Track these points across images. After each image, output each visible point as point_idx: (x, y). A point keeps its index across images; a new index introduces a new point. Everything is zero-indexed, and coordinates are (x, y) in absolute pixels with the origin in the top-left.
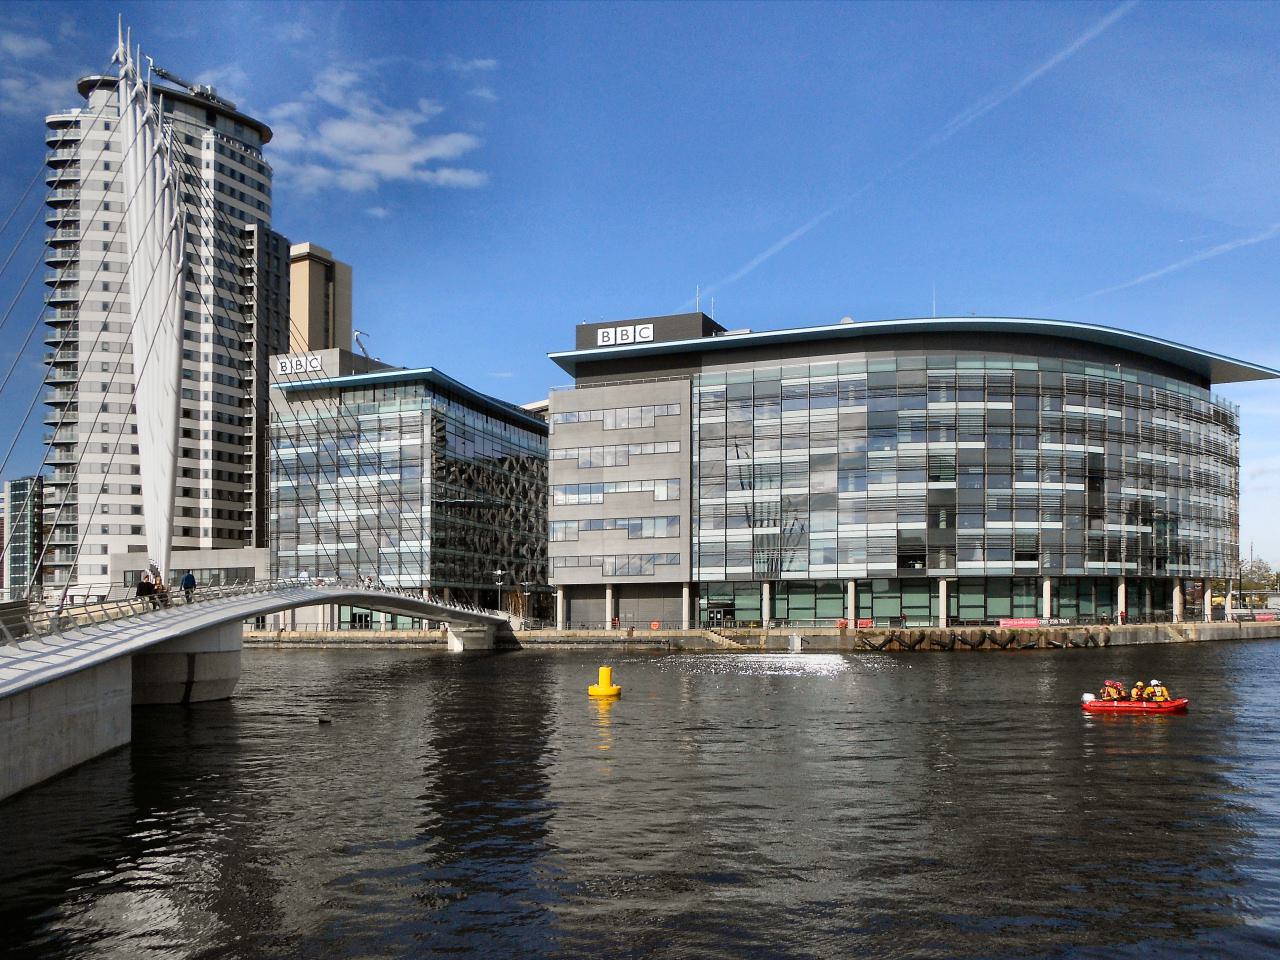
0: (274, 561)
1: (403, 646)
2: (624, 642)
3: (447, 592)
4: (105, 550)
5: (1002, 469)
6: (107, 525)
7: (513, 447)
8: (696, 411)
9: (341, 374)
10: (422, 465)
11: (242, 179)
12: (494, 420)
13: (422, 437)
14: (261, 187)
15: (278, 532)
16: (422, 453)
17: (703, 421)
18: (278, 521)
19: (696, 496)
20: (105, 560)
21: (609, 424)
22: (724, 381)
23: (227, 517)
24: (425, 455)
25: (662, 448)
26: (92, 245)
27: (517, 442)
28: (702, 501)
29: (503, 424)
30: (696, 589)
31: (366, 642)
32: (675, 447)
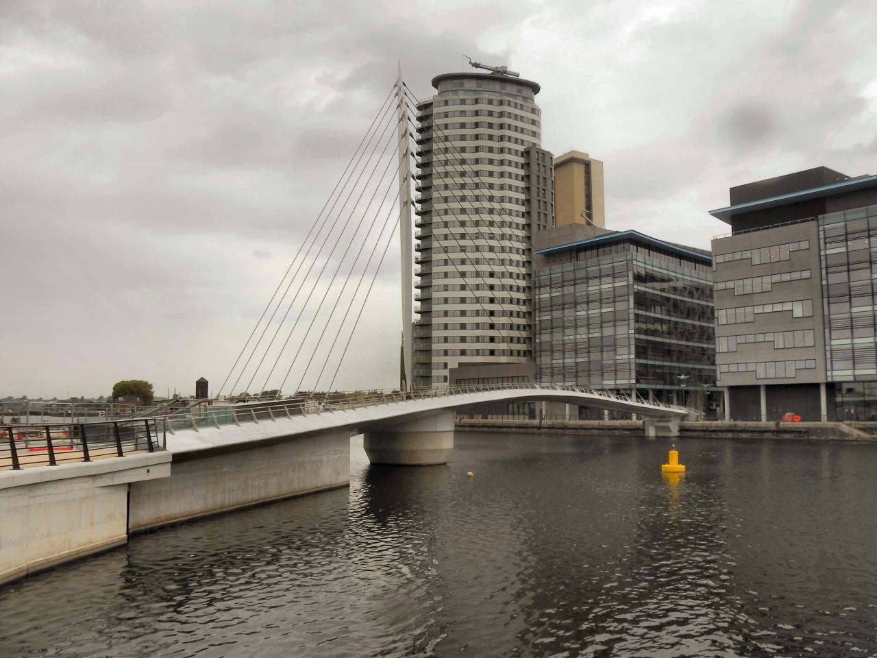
0: (538, 371)
1: (617, 433)
2: (773, 432)
3: (651, 395)
4: (446, 365)
5: (832, 239)
6: (447, 112)
7: (685, 277)
8: (822, 246)
9: (732, 204)
10: (628, 276)
11: (522, 131)
12: (655, 253)
13: (628, 281)
14: (534, 122)
15: (541, 351)
16: (628, 292)
17: (829, 252)
18: (540, 343)
19: (826, 313)
20: (446, 373)
21: (756, 261)
22: (842, 219)
23: (516, 316)
24: (630, 293)
25: (796, 276)
26: (439, 176)
27: (658, 265)
28: (832, 316)
29: (647, 251)
30: (832, 387)
31: (594, 429)
32: (806, 274)
